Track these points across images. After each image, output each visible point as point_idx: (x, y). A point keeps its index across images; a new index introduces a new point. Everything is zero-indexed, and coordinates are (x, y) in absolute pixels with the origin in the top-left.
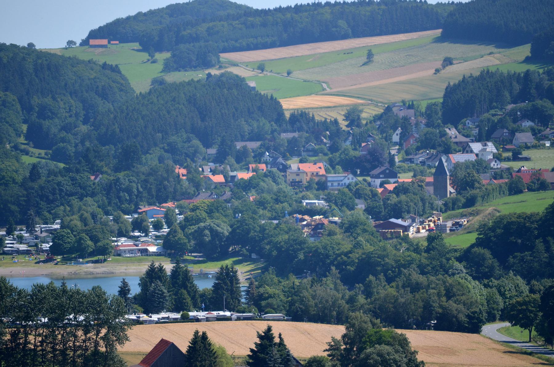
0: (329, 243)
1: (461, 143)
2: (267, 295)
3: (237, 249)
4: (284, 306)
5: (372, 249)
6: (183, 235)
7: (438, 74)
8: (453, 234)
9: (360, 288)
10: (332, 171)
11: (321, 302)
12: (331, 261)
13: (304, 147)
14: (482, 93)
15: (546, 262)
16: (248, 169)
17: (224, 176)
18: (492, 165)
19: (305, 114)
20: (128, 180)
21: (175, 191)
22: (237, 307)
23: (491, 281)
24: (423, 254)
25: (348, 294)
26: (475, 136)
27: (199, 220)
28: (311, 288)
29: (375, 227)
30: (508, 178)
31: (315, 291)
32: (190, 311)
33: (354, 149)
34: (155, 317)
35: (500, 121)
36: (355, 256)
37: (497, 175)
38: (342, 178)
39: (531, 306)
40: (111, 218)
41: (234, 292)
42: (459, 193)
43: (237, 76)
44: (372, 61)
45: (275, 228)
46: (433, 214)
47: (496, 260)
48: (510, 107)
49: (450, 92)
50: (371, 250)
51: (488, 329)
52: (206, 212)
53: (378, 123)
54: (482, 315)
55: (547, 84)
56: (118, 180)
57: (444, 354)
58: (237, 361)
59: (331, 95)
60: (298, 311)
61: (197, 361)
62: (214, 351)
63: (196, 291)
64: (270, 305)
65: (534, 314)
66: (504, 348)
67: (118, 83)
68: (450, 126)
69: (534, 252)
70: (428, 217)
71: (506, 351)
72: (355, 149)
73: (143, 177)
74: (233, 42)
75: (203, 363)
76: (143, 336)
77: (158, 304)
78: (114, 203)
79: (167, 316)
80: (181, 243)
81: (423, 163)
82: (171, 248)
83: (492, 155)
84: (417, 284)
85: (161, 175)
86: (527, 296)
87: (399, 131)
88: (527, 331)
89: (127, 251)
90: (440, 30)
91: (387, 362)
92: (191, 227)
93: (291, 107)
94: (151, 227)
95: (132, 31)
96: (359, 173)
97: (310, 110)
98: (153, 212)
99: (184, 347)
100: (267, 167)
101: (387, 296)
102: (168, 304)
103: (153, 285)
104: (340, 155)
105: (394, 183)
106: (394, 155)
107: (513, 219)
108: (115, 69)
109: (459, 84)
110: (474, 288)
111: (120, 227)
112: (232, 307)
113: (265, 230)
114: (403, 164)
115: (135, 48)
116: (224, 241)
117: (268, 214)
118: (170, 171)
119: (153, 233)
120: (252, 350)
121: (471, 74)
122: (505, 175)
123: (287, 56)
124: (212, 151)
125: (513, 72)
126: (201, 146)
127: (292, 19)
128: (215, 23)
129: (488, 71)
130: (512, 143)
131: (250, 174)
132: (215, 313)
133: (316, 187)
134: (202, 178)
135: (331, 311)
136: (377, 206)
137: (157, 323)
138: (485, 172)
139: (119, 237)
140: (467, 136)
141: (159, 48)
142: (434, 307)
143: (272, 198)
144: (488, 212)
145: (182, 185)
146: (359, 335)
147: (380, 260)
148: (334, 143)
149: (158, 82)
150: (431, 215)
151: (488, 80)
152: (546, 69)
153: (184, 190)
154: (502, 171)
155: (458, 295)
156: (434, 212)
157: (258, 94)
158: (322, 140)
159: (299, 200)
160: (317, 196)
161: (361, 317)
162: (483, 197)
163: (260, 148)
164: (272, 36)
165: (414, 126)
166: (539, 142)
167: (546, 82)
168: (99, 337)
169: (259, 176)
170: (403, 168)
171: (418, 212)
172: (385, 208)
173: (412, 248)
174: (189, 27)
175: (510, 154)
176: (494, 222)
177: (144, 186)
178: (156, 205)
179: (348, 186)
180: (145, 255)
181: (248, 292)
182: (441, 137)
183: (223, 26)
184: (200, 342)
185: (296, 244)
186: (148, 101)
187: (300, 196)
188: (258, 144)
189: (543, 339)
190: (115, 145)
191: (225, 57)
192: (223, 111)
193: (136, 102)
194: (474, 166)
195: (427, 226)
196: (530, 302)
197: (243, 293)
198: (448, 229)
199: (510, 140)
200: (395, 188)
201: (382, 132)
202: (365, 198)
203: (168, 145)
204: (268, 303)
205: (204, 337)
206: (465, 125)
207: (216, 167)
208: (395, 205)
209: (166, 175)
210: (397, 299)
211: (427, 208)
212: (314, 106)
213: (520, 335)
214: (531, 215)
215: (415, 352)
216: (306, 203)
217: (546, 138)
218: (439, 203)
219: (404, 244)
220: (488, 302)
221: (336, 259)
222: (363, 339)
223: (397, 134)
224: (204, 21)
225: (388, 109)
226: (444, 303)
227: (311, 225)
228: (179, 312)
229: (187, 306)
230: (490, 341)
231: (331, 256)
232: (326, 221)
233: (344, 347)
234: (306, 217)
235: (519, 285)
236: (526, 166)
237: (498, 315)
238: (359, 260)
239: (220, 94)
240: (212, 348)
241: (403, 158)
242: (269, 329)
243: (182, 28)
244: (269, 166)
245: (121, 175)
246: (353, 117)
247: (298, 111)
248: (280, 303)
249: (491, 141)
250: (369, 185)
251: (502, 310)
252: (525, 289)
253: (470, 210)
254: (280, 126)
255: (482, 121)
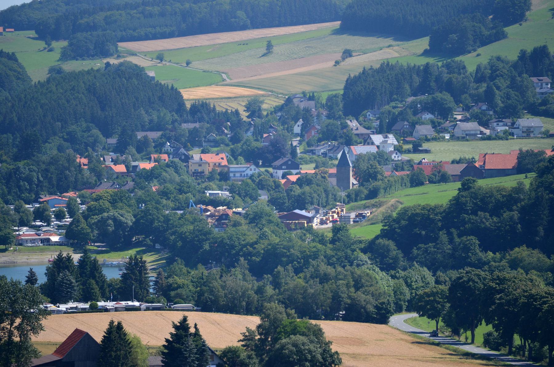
0: (234, 233)
1: (362, 134)
2: (176, 285)
3: (141, 239)
4: (192, 297)
5: (277, 240)
6: (86, 224)
7: (338, 66)
8: (356, 226)
9: (268, 279)
10: (234, 162)
11: (230, 293)
12: (237, 251)
13: (205, 137)
14: (382, 86)
15: (449, 253)
16: (150, 159)
17: (126, 166)
18: (393, 157)
19: (206, 104)
20: (29, 169)
21: (76, 181)
22: (145, 297)
23: (398, 272)
24: (328, 245)
25: (256, 284)
26: (375, 128)
27: (102, 210)
28: (220, 278)
29: (280, 217)
30: (409, 170)
31: (225, 282)
32: (98, 301)
33: (255, 140)
34: (63, 307)
35: (401, 113)
36: (261, 247)
37: (398, 167)
38: (244, 169)
39: (438, 297)
40: (12, 207)
41: (143, 283)
42: (361, 184)
43: (136, 65)
44: (272, 52)
45: (180, 219)
46: (337, 205)
47: (400, 251)
48: (410, 99)
49: (350, 83)
50: (276, 242)
51: (396, 319)
52: (110, 202)
53: (279, 114)
54: (390, 306)
55: (446, 77)
56: (18, 169)
57: (354, 345)
58: (151, 351)
59: (232, 85)
60: (207, 301)
61: (112, 351)
62: (129, 341)
63: (104, 281)
64: (179, 296)
65: (441, 305)
66: (412, 338)
67: (15, 71)
68: (350, 117)
69: (437, 244)
70: (332, 209)
71: (414, 341)
72: (257, 140)
73: (43, 167)
74: (131, 31)
75: (118, 353)
76: (56, 327)
77: (66, 294)
78: (14, 192)
79: (75, 306)
80: (84, 233)
81: (325, 154)
82: (73, 237)
83: (393, 147)
84: (325, 275)
85: (62, 165)
86: (435, 287)
87: (301, 122)
88: (434, 322)
89: (29, 241)
90: (339, 22)
91: (301, 352)
92: (95, 217)
93: (192, 97)
94: (53, 216)
95: (27, 18)
96: (261, 164)
97: (211, 101)
98: (54, 202)
99: (98, 337)
100: (169, 157)
101: (296, 287)
102: (76, 294)
103: (61, 274)
104: (242, 146)
105: (296, 174)
106: (295, 146)
107: (418, 211)
108: (12, 57)
109: (360, 77)
110: (381, 280)
111: (22, 217)
112: (141, 297)
113: (169, 220)
114: (305, 155)
115: (31, 36)
116: (128, 232)
117: (172, 205)
118: (70, 160)
119: (55, 222)
120: (167, 340)
121: (371, 66)
122: (405, 167)
123: (185, 46)
124: (113, 141)
125: (413, 65)
126: (101, 136)
127: (191, 9)
128: (112, 12)
129: (388, 64)
130: (412, 135)
131: (152, 164)
132: (123, 303)
133: (219, 177)
134: (103, 168)
135: (240, 302)
136: (280, 197)
137: (65, 313)
138: (387, 164)
139: (21, 226)
140: (368, 128)
141: (56, 37)
142: (343, 298)
143: (175, 188)
144: (390, 203)
145: (83, 175)
146: (274, 325)
147: (285, 251)
148: (235, 134)
149: (55, 71)
150: (335, 206)
151: (388, 72)
152: (445, 62)
153: (85, 180)
154: (403, 163)
155: (367, 286)
156: (338, 203)
157: (158, 84)
158: (223, 131)
159: (202, 190)
160: (220, 187)
161: (275, 307)
162: (385, 189)
163: (161, 138)
164: (171, 26)
165: (315, 118)
166: (439, 134)
167: (446, 75)
168: (14, 326)
169: (161, 167)
170: (305, 160)
171: (322, 204)
172: (289, 200)
173: (317, 239)
174: (86, 15)
175: (410, 146)
176: (399, 213)
177: (44, 175)
178: (57, 195)
179: (251, 177)
180: (47, 245)
181: (156, 283)
182: (342, 129)
183: (121, 15)
184: (116, 332)
185: (201, 235)
186: (47, 90)
187: (203, 187)
188: (159, 134)
189: (450, 330)
190: (13, 134)
191: (123, 46)
192: (123, 101)
193: (34, 90)
194: (375, 158)
195: (331, 217)
196: (437, 293)
197: (151, 284)
198: (352, 220)
199: (410, 132)
200: (298, 179)
201: (283, 123)
202: (268, 189)
203: (67, 134)
204: (177, 294)
205: (120, 327)
206: (366, 117)
207: (117, 157)
208: (299, 196)
209: (67, 165)
210: (306, 290)
211: (330, 199)
212: (214, 96)
213: (427, 325)
214: (435, 207)
215: (330, 343)
216: (210, 194)
217: (445, 130)
218: (343, 194)
219: (308, 235)
220: (395, 292)
221: (241, 249)
222: (278, 330)
223: (298, 126)
224: (102, 10)
225: (289, 101)
226: (352, 294)
227: (215, 216)
228: (87, 302)
229: (96, 296)
230: (397, 332)
231: (236, 247)
232: (230, 212)
233: (259, 337)
234: (210, 208)
235: (426, 276)
236: (427, 158)
237: (404, 305)
238: (264, 250)
239: (120, 83)
240: (127, 338)
241: (304, 149)
242: (185, 319)
243: (79, 17)
244: (171, 156)
245: (21, 164)
246: (253, 108)
247: (199, 101)
248: (190, 294)
249: (392, 133)
250: (272, 175)
251: (408, 301)
252: (431, 279)
253: (373, 201)
254: (181, 116)
255: (383, 113)
